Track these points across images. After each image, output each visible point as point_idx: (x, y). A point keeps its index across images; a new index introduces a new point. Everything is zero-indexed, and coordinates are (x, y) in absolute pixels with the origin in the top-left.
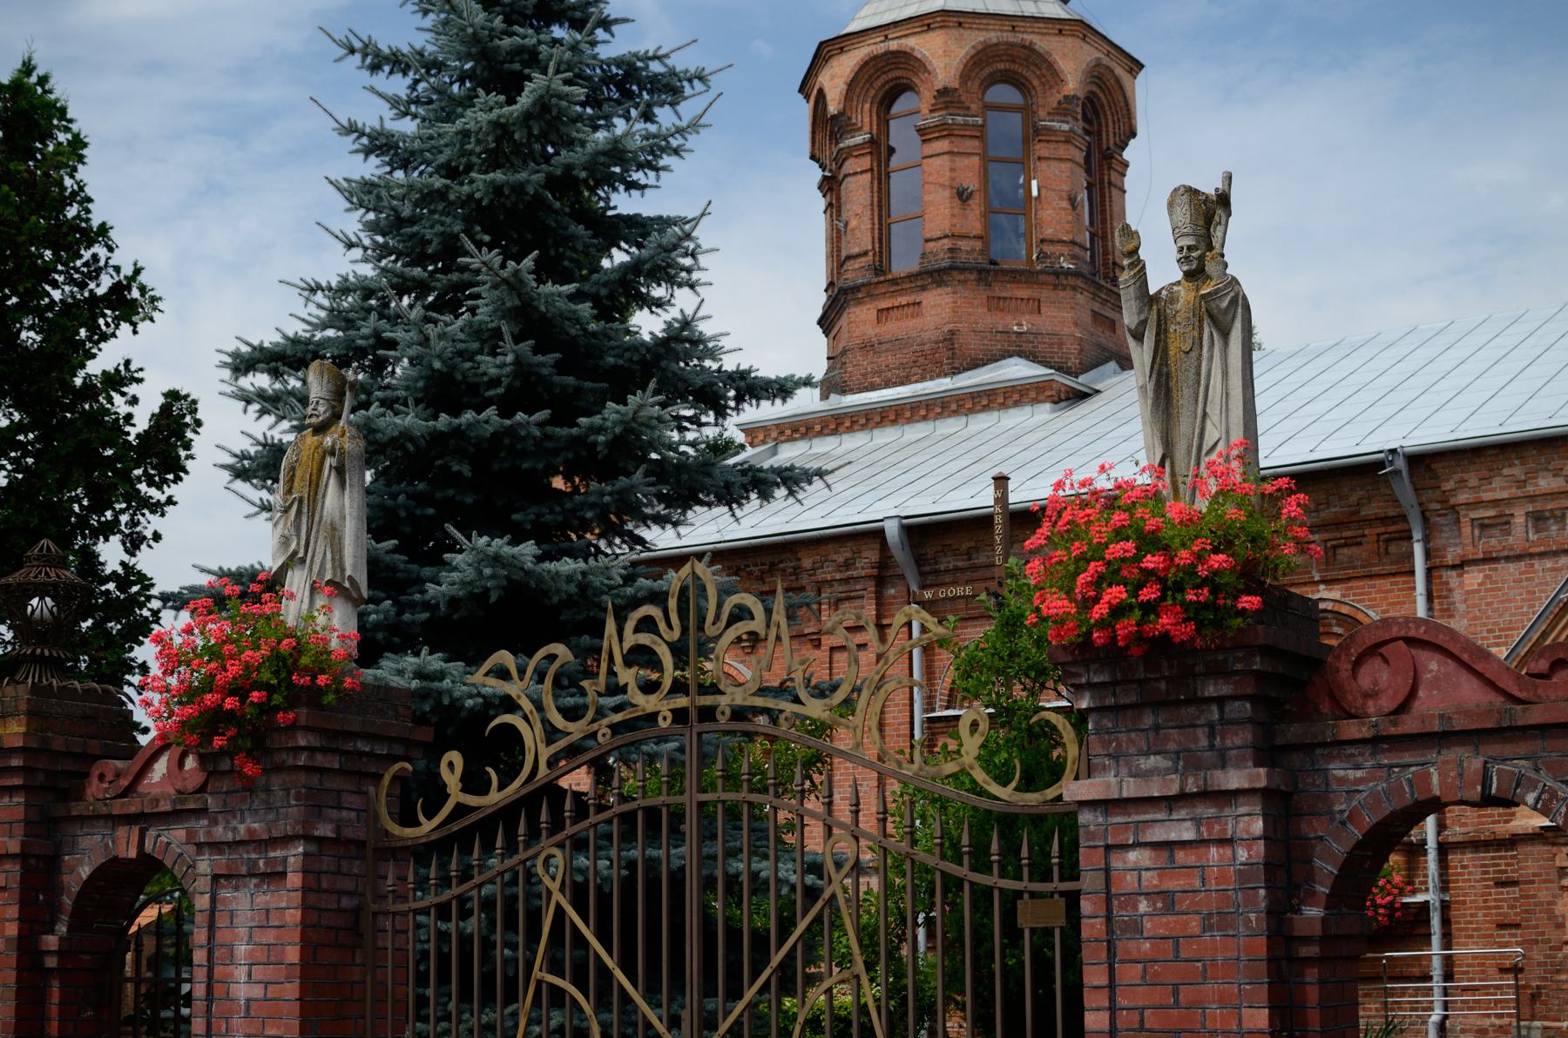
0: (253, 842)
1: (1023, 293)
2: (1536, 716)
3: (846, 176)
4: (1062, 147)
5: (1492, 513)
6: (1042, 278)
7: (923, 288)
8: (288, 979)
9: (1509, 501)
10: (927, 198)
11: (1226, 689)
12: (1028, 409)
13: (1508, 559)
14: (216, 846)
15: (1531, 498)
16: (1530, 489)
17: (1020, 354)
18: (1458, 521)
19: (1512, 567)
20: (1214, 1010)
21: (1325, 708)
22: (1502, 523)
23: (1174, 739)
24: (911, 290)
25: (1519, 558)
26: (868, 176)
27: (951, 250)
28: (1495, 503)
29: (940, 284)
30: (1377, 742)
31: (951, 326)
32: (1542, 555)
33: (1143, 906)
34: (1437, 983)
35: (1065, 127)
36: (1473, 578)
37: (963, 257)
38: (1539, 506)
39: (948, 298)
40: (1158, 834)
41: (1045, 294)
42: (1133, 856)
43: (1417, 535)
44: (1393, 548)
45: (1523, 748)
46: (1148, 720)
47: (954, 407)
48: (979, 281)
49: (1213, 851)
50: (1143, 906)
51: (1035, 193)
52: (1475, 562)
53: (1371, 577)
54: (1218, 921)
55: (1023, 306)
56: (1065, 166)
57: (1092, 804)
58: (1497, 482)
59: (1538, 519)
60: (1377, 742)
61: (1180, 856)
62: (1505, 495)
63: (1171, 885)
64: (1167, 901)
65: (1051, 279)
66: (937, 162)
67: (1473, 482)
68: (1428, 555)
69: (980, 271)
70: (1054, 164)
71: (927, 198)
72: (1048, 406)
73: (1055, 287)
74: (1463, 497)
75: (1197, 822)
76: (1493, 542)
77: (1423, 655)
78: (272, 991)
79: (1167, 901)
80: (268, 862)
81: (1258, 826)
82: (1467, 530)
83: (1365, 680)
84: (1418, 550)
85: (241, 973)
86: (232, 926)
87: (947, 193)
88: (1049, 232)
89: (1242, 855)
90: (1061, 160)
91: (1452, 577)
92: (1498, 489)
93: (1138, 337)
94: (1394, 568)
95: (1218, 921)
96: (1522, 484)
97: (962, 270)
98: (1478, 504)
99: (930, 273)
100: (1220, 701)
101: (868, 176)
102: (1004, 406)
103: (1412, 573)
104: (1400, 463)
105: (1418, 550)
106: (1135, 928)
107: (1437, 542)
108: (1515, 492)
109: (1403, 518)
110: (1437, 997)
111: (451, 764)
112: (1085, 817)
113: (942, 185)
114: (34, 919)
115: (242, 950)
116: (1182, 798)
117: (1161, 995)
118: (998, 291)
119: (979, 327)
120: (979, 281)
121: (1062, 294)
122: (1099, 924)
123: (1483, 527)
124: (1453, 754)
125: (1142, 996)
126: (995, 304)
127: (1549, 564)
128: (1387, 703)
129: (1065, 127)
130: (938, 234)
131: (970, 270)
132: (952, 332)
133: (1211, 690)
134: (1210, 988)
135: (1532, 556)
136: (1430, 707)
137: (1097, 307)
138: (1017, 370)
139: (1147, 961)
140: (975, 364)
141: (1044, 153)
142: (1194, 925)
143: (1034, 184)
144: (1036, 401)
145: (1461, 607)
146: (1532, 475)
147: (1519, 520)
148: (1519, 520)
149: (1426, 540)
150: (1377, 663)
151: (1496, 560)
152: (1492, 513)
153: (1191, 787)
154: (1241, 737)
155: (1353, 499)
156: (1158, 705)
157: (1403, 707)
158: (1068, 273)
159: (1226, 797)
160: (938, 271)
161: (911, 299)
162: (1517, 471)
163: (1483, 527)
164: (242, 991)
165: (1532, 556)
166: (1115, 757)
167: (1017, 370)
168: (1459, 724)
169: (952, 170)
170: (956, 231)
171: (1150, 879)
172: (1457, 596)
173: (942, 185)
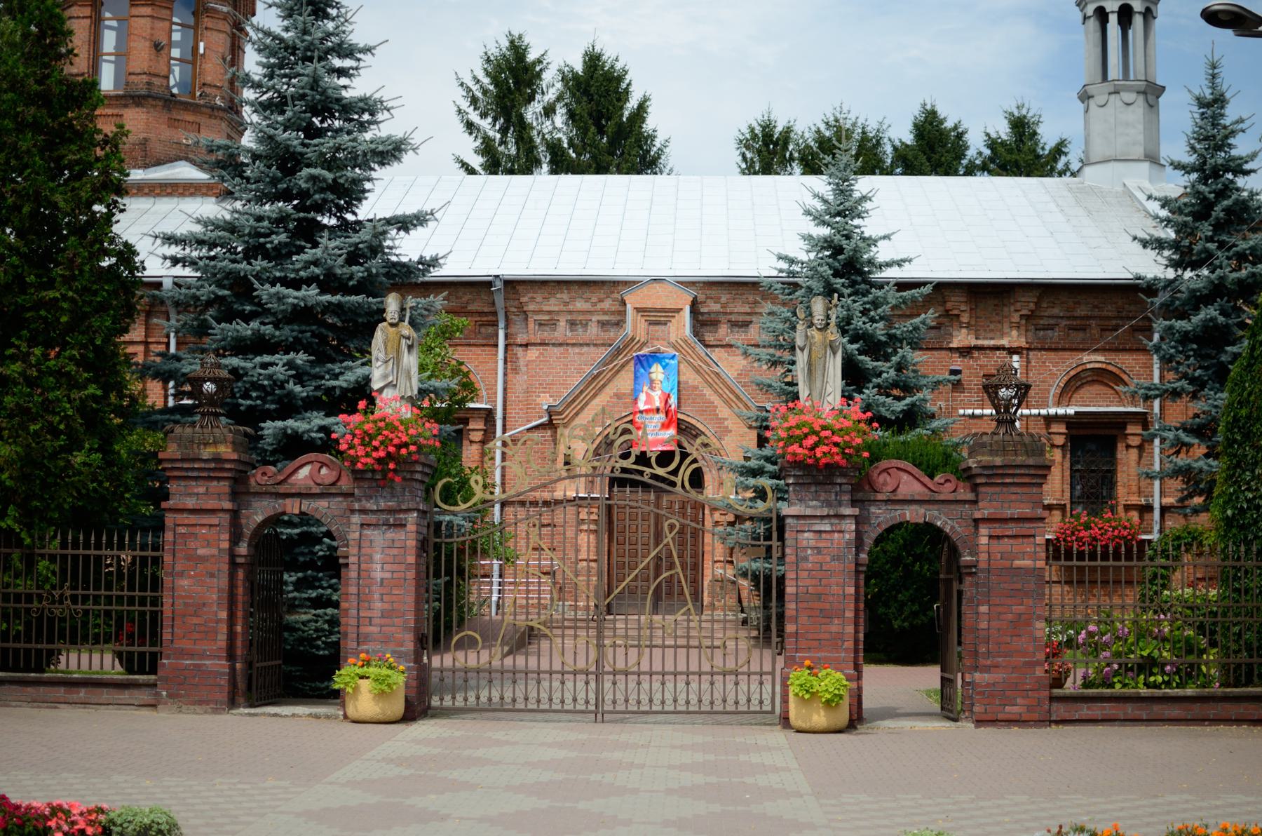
0: (391, 511)
1: (190, 118)
2: (942, 497)
3: (70, 18)
4: (221, 22)
5: (547, 317)
6: (204, 109)
7: (126, 106)
8: (408, 569)
9: (558, 312)
10: (132, 44)
11: (844, 481)
12: (199, 200)
13: (554, 345)
14: (363, 511)
15: (570, 312)
16: (571, 307)
17: (187, 159)
18: (526, 319)
19: (556, 350)
20: (834, 587)
21: (867, 487)
22: (552, 324)
23: (823, 496)
24: (117, 106)
25: (560, 345)
26: (88, 21)
27: (149, 84)
28: (550, 312)
29: (138, 105)
30: (887, 502)
31: (145, 135)
32: (574, 345)
33: (809, 552)
34: (496, 579)
35: (225, 9)
36: (533, 353)
37: (155, 90)
38: (574, 317)
39: (144, 116)
40: (817, 528)
41: (203, 120)
42: (806, 535)
43: (502, 325)
44: (483, 330)
45: (936, 507)
46: (813, 489)
47: (146, 191)
48: (164, 107)
49: (836, 535)
50: (809, 552)
51: (201, 51)
52: (534, 344)
53: (469, 345)
54: (837, 558)
55: (189, 127)
56: (222, 36)
57: (793, 516)
58: (552, 301)
59: (572, 324)
60: (887, 502)
61: (824, 535)
62: (556, 308)
63: (821, 545)
64: (818, 550)
65: (209, 111)
66: (142, 21)
67: (539, 299)
68: (506, 336)
69: (166, 100)
70: (215, 33)
71: (132, 44)
72: (213, 199)
73: (210, 117)
74: (531, 307)
75: (832, 525)
76: (546, 334)
77: (902, 474)
78: (395, 575)
79: (818, 550)
80: (395, 519)
81: (853, 527)
82: (531, 325)
83: (881, 479)
84: (501, 334)
85: (379, 567)
86: (371, 546)
87: (147, 44)
88: (209, 79)
89: (847, 536)
90: (219, 31)
91: (520, 351)
92: (553, 304)
93: (802, 349)
94: (484, 342)
95: (837, 558)
96: (566, 304)
97: (155, 98)
98: (540, 312)
99: (132, 97)
100: (840, 485)
101: (88, 21)
102: (182, 195)
103: (497, 346)
104: (499, 285)
105: (501, 334)
106: (806, 559)
107: (512, 330)
108: (562, 308)
109: (495, 313)
110: (496, 587)
111: (476, 482)
112: (788, 521)
113: (145, 38)
114: (235, 539)
115: (378, 557)
116: (828, 516)
117: (814, 582)
118: (175, 115)
119: (163, 138)
120: (164, 107)
121: (214, 121)
122: (793, 557)
123: (540, 325)
124: (915, 507)
125: (808, 582)
126: (173, 123)
127: (577, 350)
128: (890, 489)
129: (225, 9)
130: (139, 71)
131: (160, 99)
132: (146, 140)
133: (839, 481)
134: (833, 580)
135: (567, 344)
136: (903, 492)
137: (229, 130)
138: (185, 172)
139: (810, 570)
140: (159, 163)
141: (210, 25)
142: (828, 559)
143: (202, 45)
144: (206, 195)
145: (524, 369)
146: (573, 299)
147: (562, 324)
148: (562, 324)
149: (507, 327)
150: (885, 475)
151: (547, 344)
152: (547, 317)
153: (832, 513)
154: (846, 497)
155: (465, 299)
156: (817, 484)
157: (894, 491)
158: (220, 108)
159: (843, 517)
160: (139, 97)
161: (115, 111)
162: (565, 296)
163: (540, 325)
164: (378, 575)
165: (567, 344)
166: (800, 500)
167: (185, 172)
168: (917, 498)
169: (152, 29)
170: (153, 70)
171: (812, 543)
172: (522, 362)
173: (145, 38)
